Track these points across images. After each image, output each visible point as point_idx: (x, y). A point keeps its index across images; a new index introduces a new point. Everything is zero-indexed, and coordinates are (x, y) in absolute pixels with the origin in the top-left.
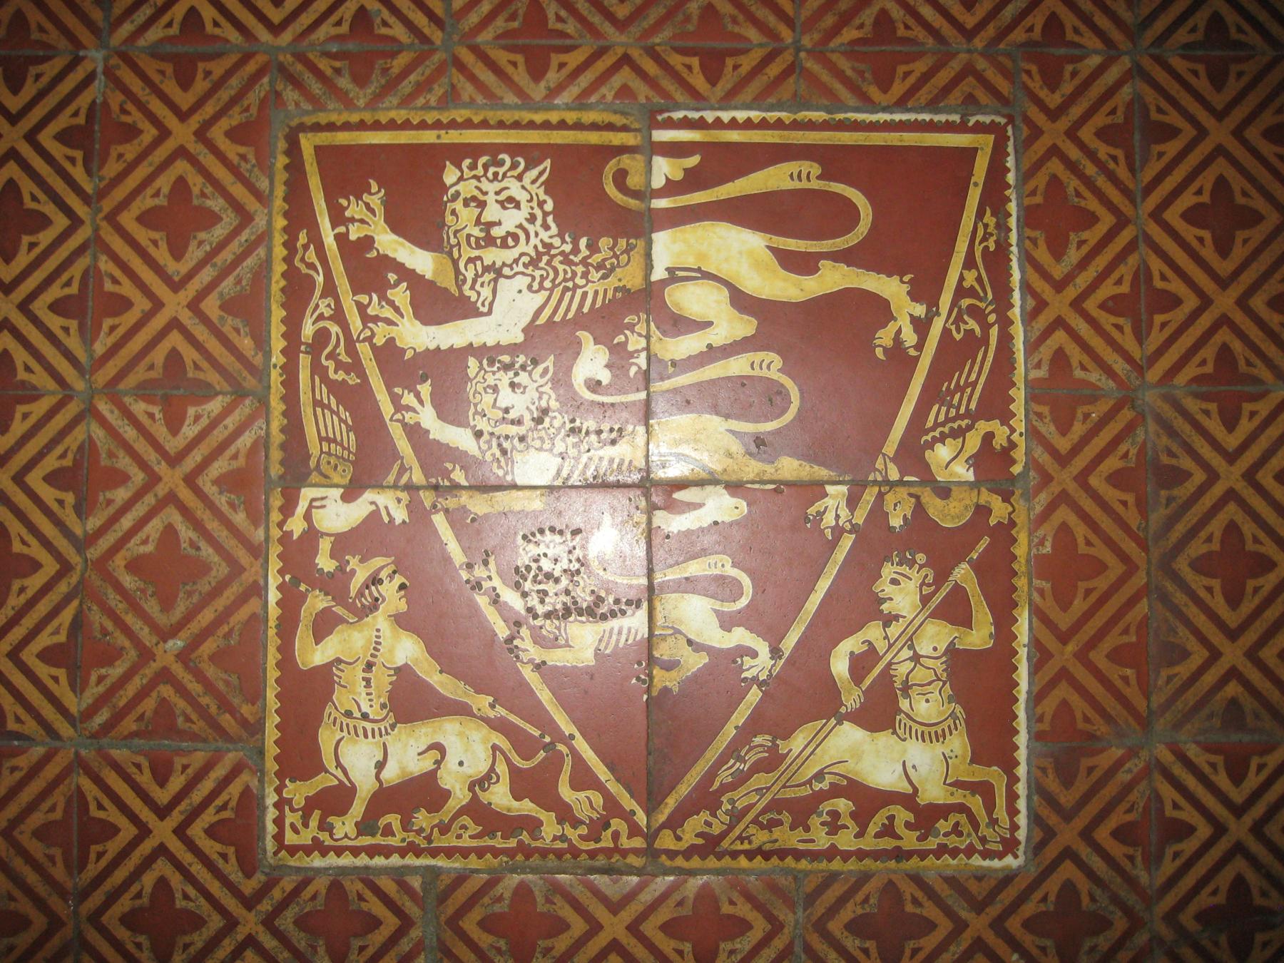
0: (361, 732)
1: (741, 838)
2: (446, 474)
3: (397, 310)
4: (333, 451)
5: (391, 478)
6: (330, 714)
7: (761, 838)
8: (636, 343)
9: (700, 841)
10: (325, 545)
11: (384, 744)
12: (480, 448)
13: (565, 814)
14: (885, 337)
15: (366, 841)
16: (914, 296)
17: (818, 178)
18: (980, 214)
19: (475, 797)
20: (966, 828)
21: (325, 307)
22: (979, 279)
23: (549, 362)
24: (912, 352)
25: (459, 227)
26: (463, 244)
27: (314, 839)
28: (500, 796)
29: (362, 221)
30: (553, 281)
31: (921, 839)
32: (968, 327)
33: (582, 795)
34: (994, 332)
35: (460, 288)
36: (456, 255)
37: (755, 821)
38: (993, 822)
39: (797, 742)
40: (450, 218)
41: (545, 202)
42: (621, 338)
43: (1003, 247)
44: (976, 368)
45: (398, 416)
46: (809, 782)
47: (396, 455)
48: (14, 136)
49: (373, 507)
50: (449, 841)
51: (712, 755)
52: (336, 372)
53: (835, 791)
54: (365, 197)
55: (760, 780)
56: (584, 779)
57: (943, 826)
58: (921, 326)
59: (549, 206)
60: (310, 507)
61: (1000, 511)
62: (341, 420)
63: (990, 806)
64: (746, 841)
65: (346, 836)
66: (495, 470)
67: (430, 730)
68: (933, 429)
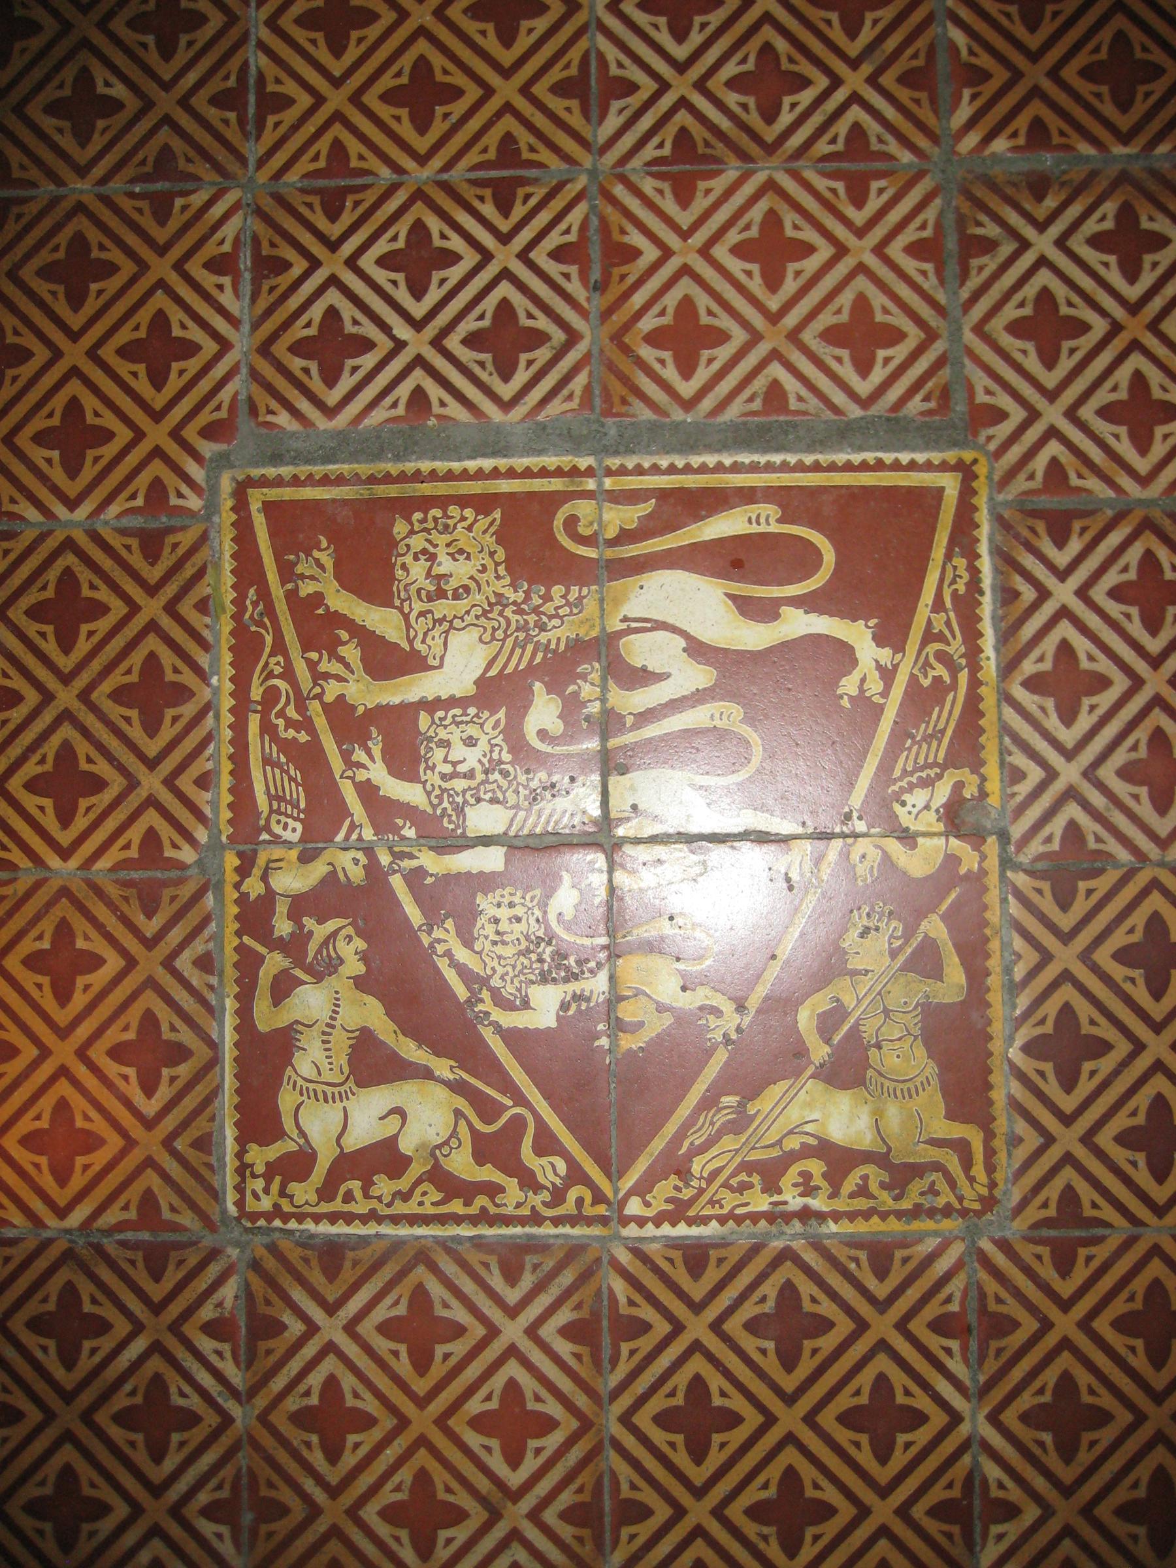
0: (321, 1097)
1: (712, 1202)
2: (397, 830)
3: (347, 666)
4: (289, 812)
5: (340, 837)
6: (290, 1077)
7: (730, 1201)
8: (587, 690)
9: (670, 1207)
10: (282, 908)
11: (345, 1108)
12: (430, 802)
13: (529, 1181)
14: (849, 686)
15: (325, 1208)
16: (880, 640)
17: (779, 521)
18: (949, 556)
19: (437, 1166)
20: (942, 1185)
21: (276, 664)
22: (948, 623)
23: (501, 714)
24: (878, 699)
25: (409, 580)
26: (414, 598)
27: (276, 1206)
28: (461, 1163)
29: (312, 578)
30: (505, 632)
31: (897, 1198)
32: (935, 673)
33: (544, 1161)
34: (963, 677)
35: (411, 642)
36: (406, 610)
37: (726, 1185)
38: (972, 1180)
39: (763, 1104)
40: (400, 572)
41: (495, 552)
42: (572, 688)
43: (974, 584)
44: (945, 714)
45: (349, 773)
46: (779, 1142)
47: (345, 812)
48: (1156, 1231)
49: (330, 868)
50: (410, 1208)
51: (684, 1111)
52: (286, 730)
53: (806, 1152)
54: (316, 554)
55: (729, 1143)
56: (546, 1144)
57: (916, 1187)
58: (887, 675)
59: (501, 555)
60: (267, 868)
61: (970, 860)
62: (291, 779)
63: (967, 1164)
64: (717, 1206)
65: (307, 1203)
66: (446, 824)
67: (415, 1089)
68: (900, 779)
